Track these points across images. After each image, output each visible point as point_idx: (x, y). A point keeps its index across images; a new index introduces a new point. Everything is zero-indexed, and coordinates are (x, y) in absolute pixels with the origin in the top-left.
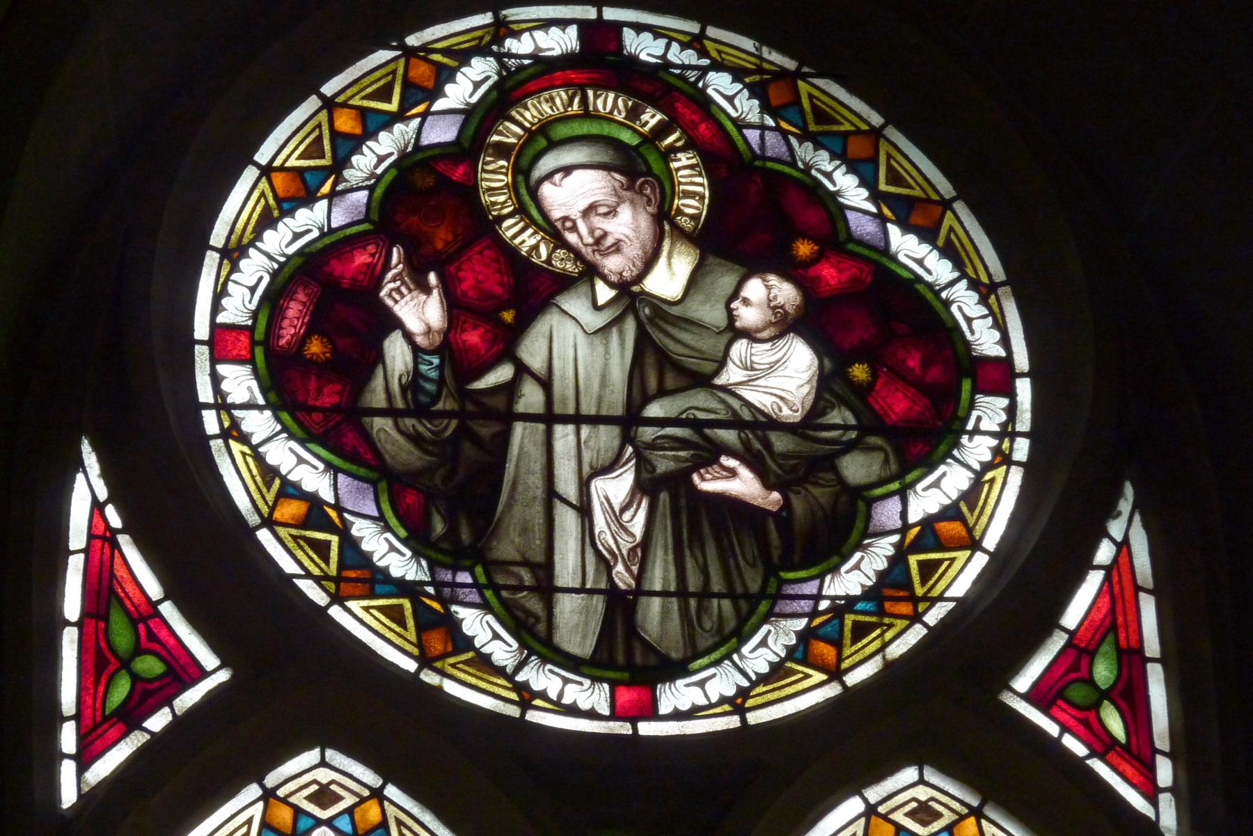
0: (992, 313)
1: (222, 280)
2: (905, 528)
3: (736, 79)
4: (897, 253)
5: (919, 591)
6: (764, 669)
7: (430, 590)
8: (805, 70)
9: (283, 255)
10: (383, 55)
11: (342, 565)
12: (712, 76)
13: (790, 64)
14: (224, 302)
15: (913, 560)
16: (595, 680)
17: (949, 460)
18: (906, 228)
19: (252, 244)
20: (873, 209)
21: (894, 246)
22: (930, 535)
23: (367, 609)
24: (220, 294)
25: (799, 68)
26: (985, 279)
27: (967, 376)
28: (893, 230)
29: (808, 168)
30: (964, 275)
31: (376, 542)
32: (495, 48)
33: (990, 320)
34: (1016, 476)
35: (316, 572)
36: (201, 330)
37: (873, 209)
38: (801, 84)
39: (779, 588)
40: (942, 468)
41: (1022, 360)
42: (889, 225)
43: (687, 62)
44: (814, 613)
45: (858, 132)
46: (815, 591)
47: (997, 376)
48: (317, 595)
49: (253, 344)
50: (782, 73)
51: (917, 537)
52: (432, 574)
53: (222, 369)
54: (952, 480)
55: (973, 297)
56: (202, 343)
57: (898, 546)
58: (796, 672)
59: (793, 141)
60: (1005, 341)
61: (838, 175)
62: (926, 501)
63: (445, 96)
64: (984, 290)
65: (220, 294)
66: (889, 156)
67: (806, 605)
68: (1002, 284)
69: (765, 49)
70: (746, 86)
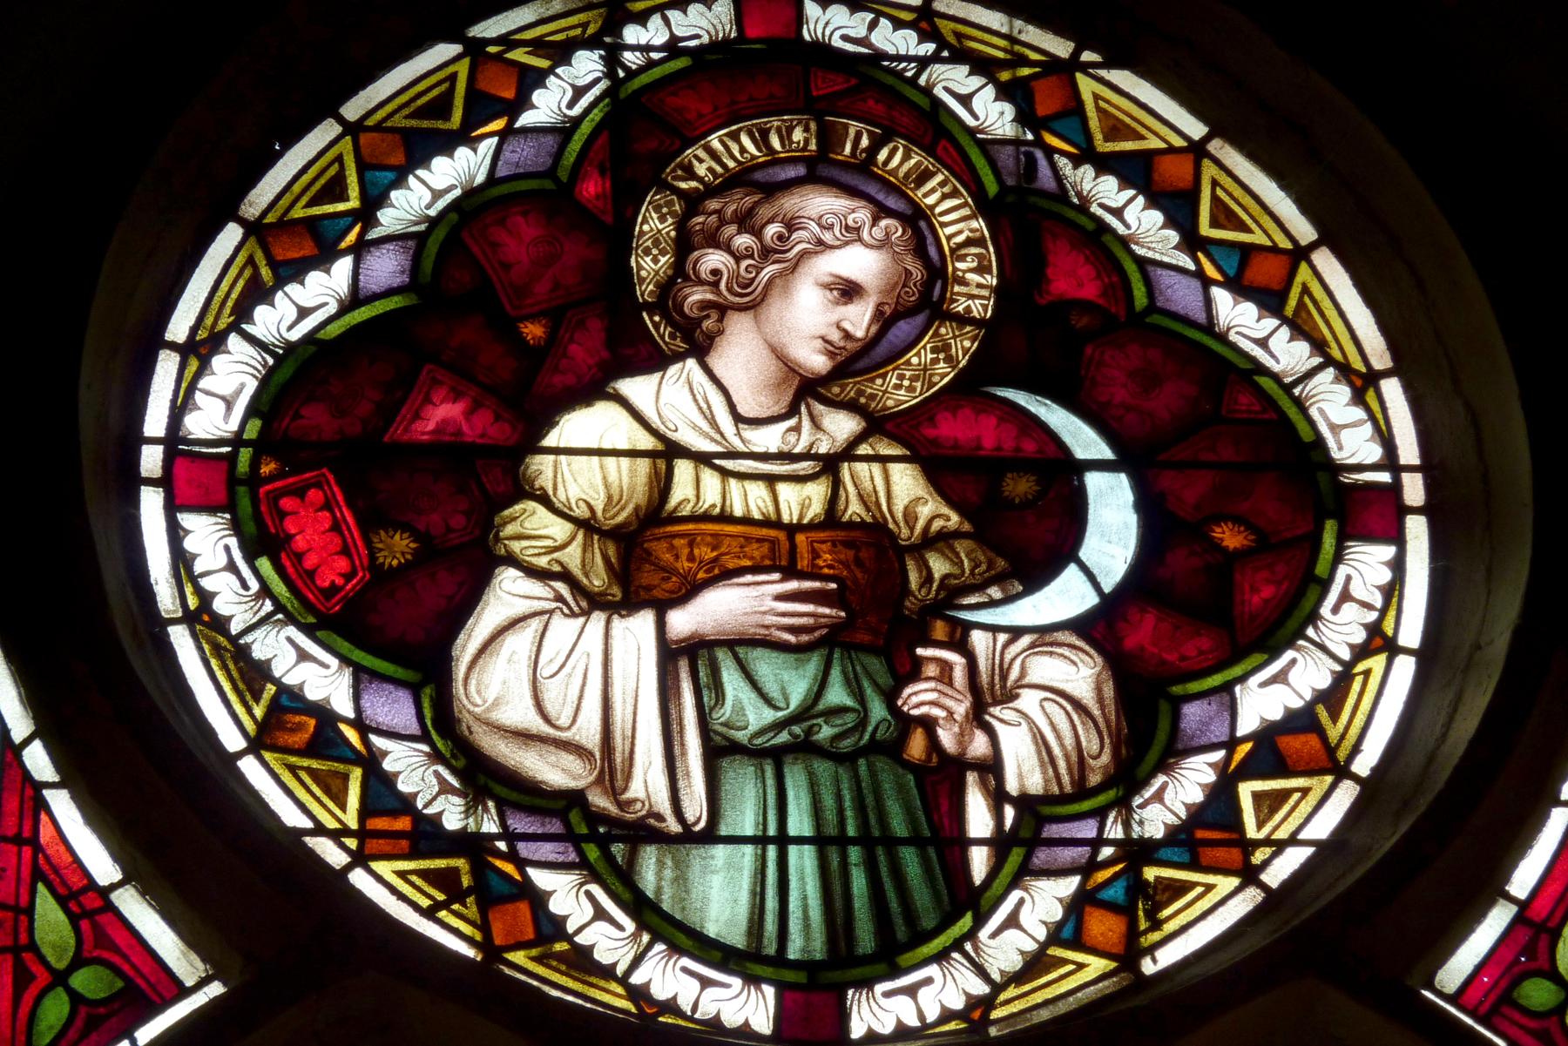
0: (194, 579)
1: (184, 385)
2: (1231, 744)
3: (585, 953)
4: (340, 668)
5: (1252, 832)
6: (1014, 963)
7: (502, 846)
8: (1088, 56)
9: (1299, 649)
10: (444, 51)
11: (365, 813)
12: (938, 69)
13: (1062, 48)
14: (1386, 576)
15: (1246, 790)
16: (752, 980)
17: (1301, 642)
18: (324, 715)
19: (1348, 666)
20: (375, 739)
21: (345, 679)
22: (1273, 751)
23: (402, 875)
24: (1393, 591)
25: (1076, 54)
26: (1358, 365)
27: (1331, 517)
28: (1221, 296)
29: (1085, 201)
30: (234, 640)
31: (1145, 226)
32: (608, 40)
33: (198, 568)
34: (1405, 668)
35: (332, 824)
36: (1417, 529)
37: (375, 739)
38: (1079, 76)
39: (1039, 830)
40: (1289, 655)
41: (151, 503)
42: (351, 715)
43: (903, 52)
44: (1088, 868)
45: (1172, 150)
46: (1092, 834)
47: (197, 478)
48: (334, 856)
49: (233, 481)
50: (1053, 65)
51: (1249, 754)
52: (503, 823)
53: (187, 520)
54: (1305, 674)
55: (220, 606)
56: (151, 482)
57: (1222, 768)
58: (1065, 962)
59: (1063, 163)
60: (175, 534)
61: (1131, 214)
62: (1261, 702)
63: (533, 107)
64: (1359, 382)
65: (1393, 591)
66: (1215, 183)
67: (1080, 854)
68: (1386, 374)
69: (1018, 23)
70: (569, 938)
